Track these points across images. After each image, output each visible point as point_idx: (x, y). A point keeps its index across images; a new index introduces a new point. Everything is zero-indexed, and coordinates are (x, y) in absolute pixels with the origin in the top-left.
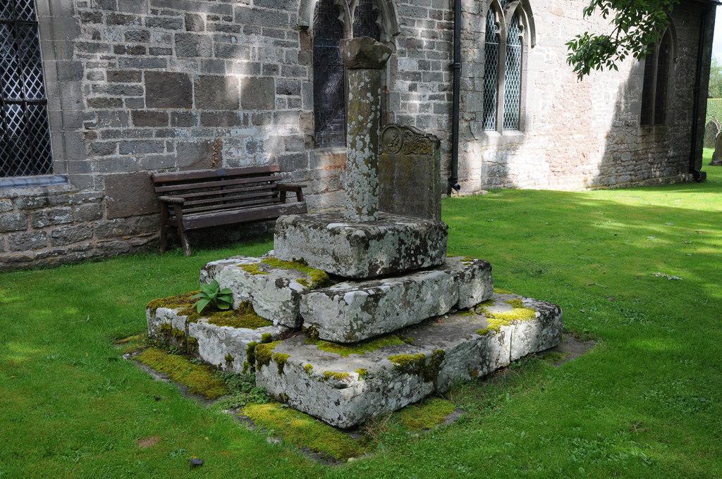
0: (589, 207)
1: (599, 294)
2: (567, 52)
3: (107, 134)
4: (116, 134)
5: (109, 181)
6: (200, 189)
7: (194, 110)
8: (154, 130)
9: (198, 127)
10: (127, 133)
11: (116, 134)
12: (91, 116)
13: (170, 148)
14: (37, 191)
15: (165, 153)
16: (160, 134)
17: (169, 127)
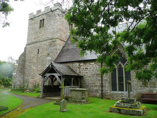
0: (125, 73)
1: (107, 102)
2: (14, 8)
3: (137, 88)
4: (138, 88)
5: (137, 93)
6: (148, 96)
7: (148, 85)
8: (143, 88)
9: (149, 88)
10: (139, 88)
11: (138, 88)
12: (135, 86)
13: (145, 90)
14: (121, 93)
15: (144, 91)
16: (143, 88)
17: (145, 87)
